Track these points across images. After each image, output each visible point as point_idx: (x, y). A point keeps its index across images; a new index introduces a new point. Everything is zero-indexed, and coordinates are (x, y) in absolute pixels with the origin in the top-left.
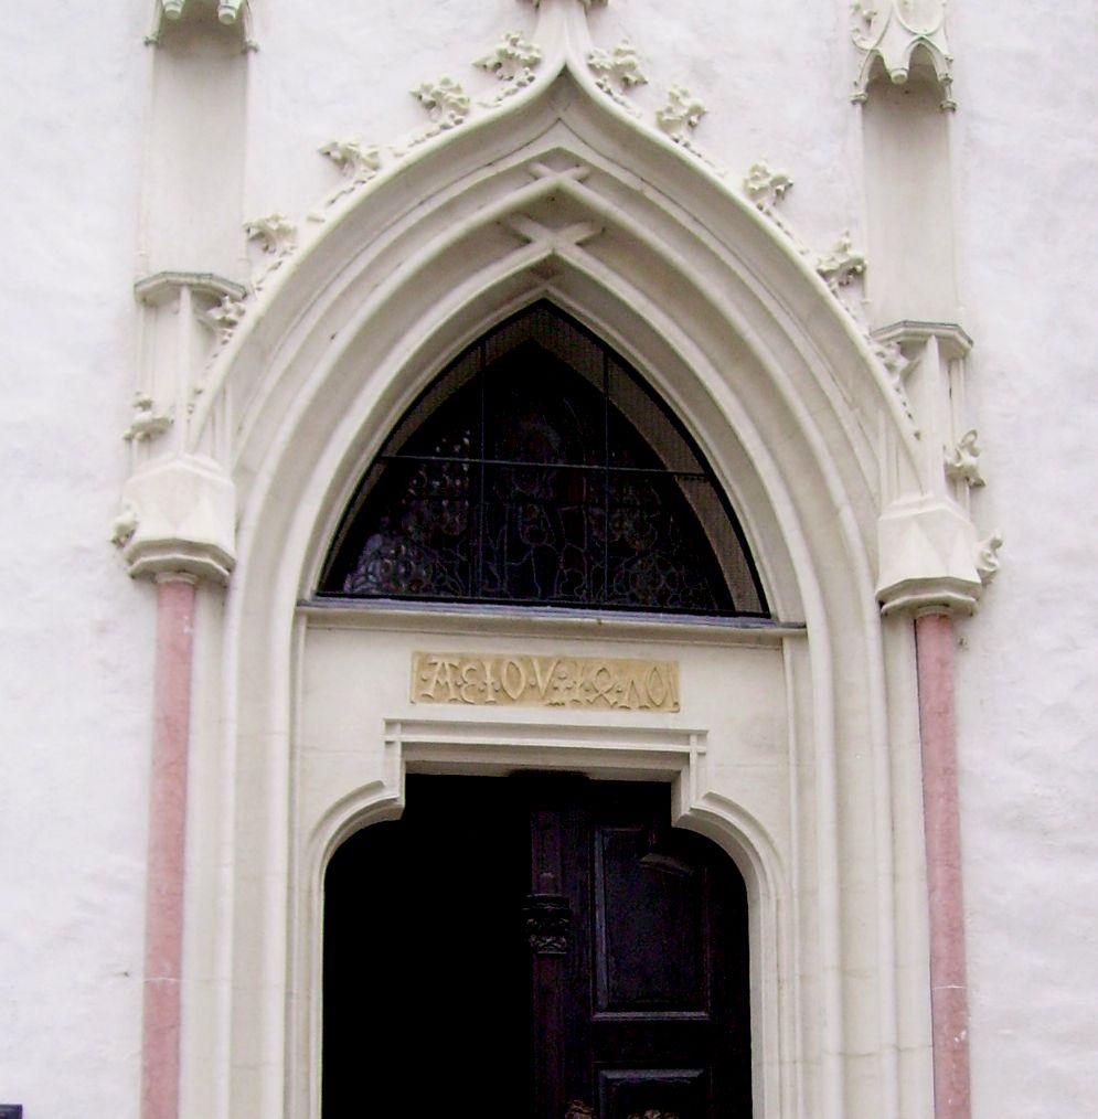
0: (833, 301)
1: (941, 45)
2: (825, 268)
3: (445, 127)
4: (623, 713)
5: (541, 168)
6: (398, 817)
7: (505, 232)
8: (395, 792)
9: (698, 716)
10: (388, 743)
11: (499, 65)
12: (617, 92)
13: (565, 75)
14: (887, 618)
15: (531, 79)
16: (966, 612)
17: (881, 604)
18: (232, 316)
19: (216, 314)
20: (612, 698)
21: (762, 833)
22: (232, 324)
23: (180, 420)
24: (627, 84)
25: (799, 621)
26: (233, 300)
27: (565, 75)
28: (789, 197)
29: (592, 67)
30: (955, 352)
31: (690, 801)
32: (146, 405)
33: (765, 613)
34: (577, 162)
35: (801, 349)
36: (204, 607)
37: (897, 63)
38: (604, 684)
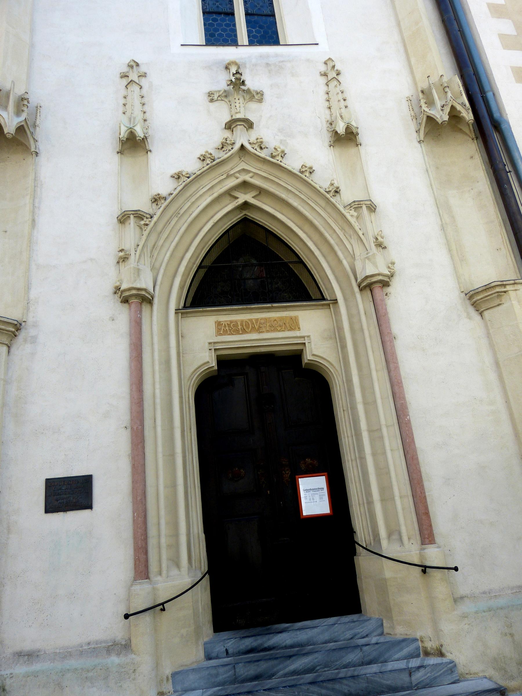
0: (331, 199)
1: (354, 123)
2: (327, 190)
3: (208, 164)
4: (283, 332)
5: (238, 175)
6: (216, 374)
7: (229, 194)
8: (214, 364)
9: (306, 330)
10: (210, 349)
11: (223, 147)
12: (258, 149)
13: (242, 146)
14: (361, 289)
15: (232, 148)
16: (385, 284)
17: (359, 287)
18: (147, 222)
19: (143, 222)
20: (279, 329)
21: (332, 365)
22: (147, 225)
23: (133, 253)
24: (261, 148)
25: (335, 299)
26: (147, 218)
27: (242, 146)
28: (313, 174)
29: (250, 143)
30: (372, 208)
31: (308, 357)
32: (122, 251)
33: (323, 299)
34: (248, 172)
35: (324, 216)
36: (146, 308)
37: (341, 129)
38: (276, 324)
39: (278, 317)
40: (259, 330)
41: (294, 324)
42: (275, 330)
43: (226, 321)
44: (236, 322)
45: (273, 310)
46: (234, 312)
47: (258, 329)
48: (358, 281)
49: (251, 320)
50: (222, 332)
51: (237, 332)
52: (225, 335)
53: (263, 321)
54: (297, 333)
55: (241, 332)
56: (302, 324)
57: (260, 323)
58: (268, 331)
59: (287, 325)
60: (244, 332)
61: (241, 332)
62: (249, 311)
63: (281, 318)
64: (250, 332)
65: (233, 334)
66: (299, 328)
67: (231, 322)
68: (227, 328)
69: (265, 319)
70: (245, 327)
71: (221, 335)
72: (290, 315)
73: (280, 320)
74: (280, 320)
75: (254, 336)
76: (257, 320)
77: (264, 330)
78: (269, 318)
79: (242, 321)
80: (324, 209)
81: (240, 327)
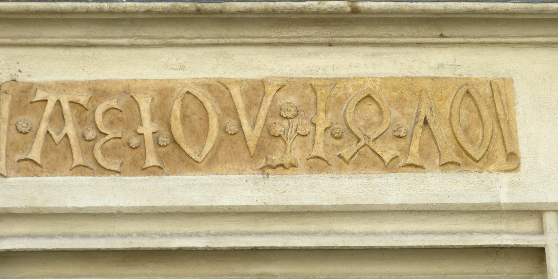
4: (410, 176)
38: (370, 124)
39: (386, 81)
40: (264, 158)
41: (481, 132)
42: (365, 159)
43: (65, 86)
44: (128, 92)
45: (359, 32)
46: (119, 35)
47: (260, 147)
48: (458, 160)
49: (219, 89)
50: (35, 154)
51: (132, 161)
52: (53, 171)
53: (293, 99)
54: (500, 188)
55: (152, 160)
56: (531, 130)
57: (276, 112)
58: (318, 164)
59: (442, 132)
60: (174, 157)
61: (152, 160)
62: (211, 33)
63: (407, 90)
64: (211, 163)
65: (104, 171)
66: (512, 156)
67: (98, 92)
68: (70, 129)
69: (310, 86)
70: (178, 131)
71: (29, 167)
72: (462, 72)
73: (401, 102)
74: (401, 102)
75: (237, 188)
76: (256, 90)
77: (296, 154)
78: (335, 82)
79: (164, 94)
80: (403, 36)
81: (148, 128)
